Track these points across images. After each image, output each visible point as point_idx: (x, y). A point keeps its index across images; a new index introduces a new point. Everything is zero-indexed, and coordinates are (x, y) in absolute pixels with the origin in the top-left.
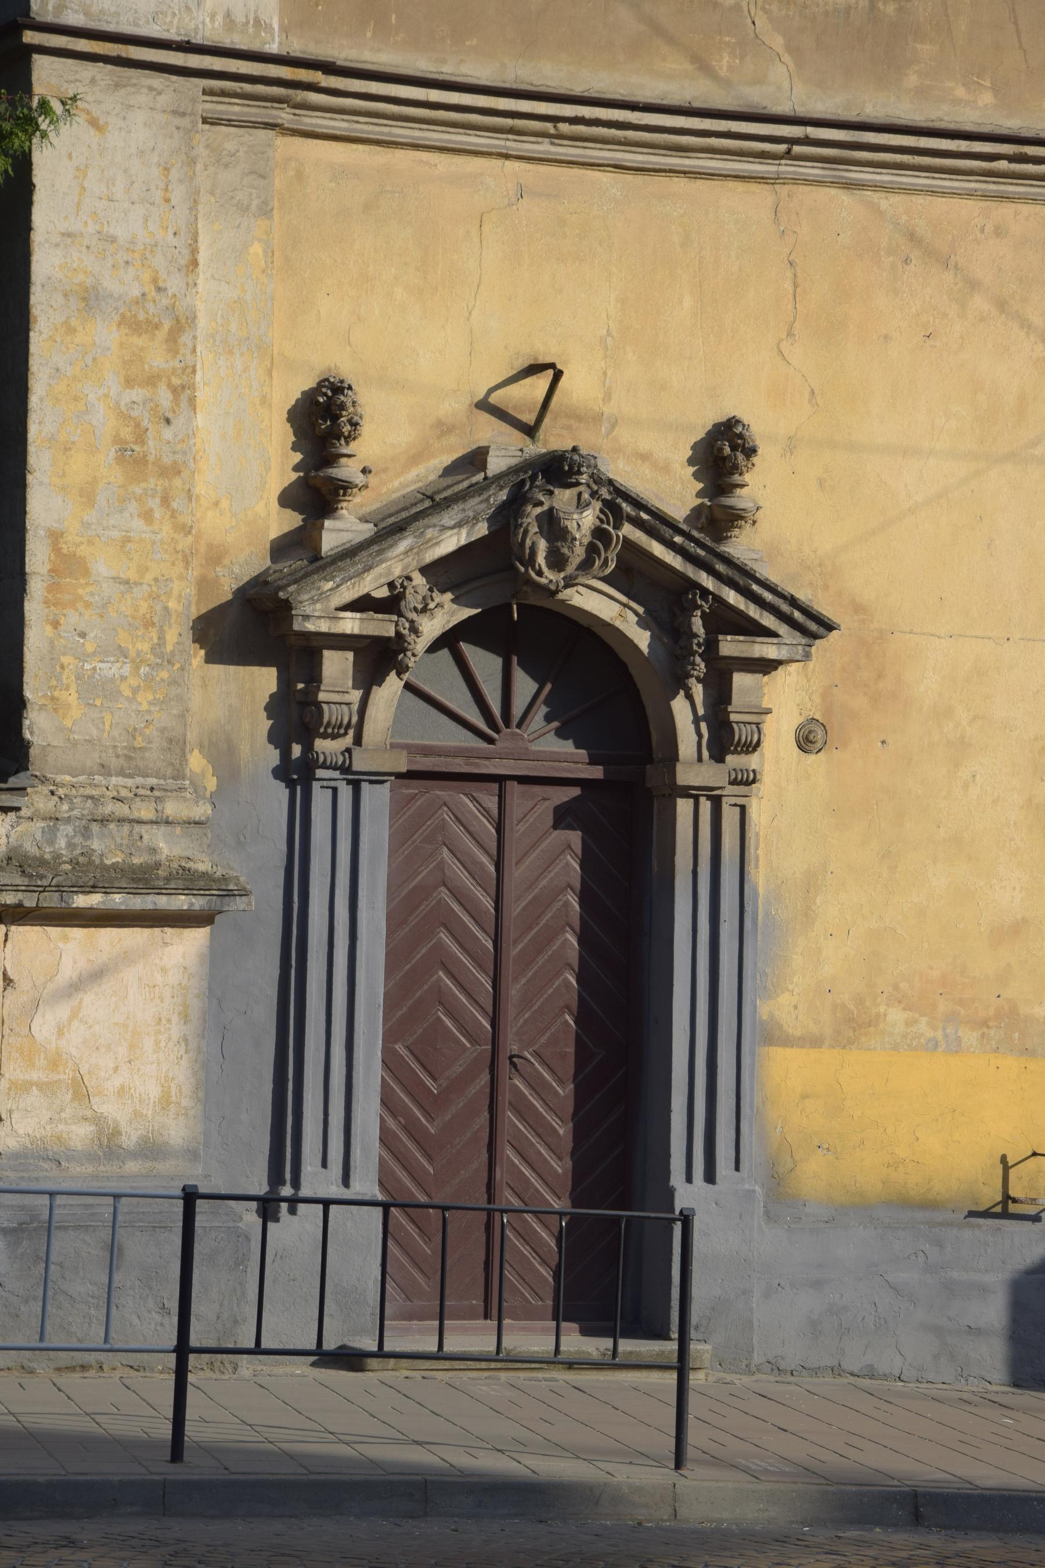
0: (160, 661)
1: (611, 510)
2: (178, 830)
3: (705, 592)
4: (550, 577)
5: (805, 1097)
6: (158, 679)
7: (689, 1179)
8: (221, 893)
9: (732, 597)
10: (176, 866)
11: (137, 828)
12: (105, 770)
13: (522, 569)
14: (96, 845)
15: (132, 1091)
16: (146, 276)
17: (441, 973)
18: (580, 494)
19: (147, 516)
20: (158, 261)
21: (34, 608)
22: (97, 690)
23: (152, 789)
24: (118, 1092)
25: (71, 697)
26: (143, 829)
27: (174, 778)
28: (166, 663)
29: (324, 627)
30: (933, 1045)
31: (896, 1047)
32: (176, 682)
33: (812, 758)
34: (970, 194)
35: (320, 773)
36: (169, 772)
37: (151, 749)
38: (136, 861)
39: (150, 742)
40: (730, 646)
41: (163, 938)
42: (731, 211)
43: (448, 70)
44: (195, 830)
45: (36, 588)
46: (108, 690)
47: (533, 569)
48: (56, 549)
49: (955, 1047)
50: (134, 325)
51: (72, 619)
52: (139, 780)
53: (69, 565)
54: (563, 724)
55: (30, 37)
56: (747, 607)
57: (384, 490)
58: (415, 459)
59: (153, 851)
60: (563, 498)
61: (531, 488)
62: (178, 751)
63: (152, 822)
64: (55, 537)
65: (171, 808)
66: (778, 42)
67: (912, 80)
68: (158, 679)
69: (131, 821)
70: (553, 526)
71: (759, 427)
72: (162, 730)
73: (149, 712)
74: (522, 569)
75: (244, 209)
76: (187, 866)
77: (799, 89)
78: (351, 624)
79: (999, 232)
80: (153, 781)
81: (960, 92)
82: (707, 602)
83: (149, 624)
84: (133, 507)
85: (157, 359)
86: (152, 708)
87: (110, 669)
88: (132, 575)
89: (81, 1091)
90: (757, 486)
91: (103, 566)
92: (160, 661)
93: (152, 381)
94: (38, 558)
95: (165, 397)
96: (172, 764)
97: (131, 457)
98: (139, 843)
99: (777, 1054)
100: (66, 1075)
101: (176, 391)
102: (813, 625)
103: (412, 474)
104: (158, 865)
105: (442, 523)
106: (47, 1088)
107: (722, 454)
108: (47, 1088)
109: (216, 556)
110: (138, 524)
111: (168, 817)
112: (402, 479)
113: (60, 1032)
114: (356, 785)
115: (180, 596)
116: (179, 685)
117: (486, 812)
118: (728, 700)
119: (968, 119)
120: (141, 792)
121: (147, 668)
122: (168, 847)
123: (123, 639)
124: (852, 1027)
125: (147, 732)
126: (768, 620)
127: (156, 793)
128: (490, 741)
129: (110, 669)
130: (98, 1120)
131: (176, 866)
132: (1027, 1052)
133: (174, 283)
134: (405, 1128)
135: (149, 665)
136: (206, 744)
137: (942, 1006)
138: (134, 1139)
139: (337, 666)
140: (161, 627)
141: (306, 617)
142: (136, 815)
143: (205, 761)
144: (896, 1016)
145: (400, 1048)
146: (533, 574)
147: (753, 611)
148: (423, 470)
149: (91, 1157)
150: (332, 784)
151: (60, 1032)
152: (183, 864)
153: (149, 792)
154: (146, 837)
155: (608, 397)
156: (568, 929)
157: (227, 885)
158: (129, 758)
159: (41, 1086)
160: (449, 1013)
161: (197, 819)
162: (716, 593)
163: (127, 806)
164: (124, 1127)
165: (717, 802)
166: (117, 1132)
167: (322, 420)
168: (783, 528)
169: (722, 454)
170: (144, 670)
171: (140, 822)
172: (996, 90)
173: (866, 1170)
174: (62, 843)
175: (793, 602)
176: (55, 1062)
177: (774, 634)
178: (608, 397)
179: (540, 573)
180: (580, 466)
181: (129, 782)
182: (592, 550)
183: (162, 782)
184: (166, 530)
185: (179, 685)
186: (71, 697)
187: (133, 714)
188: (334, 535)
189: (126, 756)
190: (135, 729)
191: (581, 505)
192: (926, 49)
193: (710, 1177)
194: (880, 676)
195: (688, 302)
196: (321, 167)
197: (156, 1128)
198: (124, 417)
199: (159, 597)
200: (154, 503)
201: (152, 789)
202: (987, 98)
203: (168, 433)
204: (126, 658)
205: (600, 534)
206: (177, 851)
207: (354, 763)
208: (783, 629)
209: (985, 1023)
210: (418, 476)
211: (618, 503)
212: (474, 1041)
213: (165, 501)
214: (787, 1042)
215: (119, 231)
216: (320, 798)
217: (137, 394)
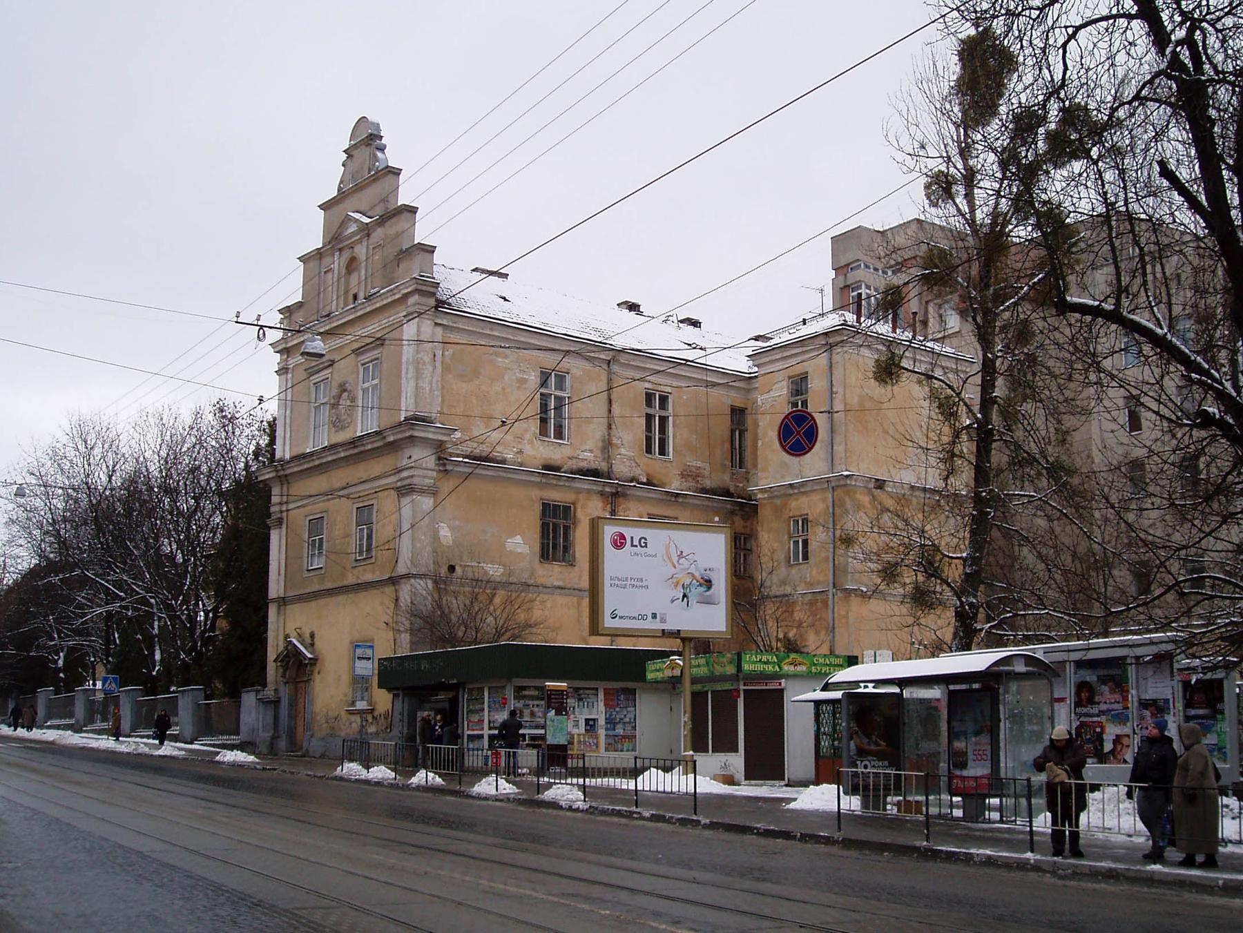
169: (312, 636)
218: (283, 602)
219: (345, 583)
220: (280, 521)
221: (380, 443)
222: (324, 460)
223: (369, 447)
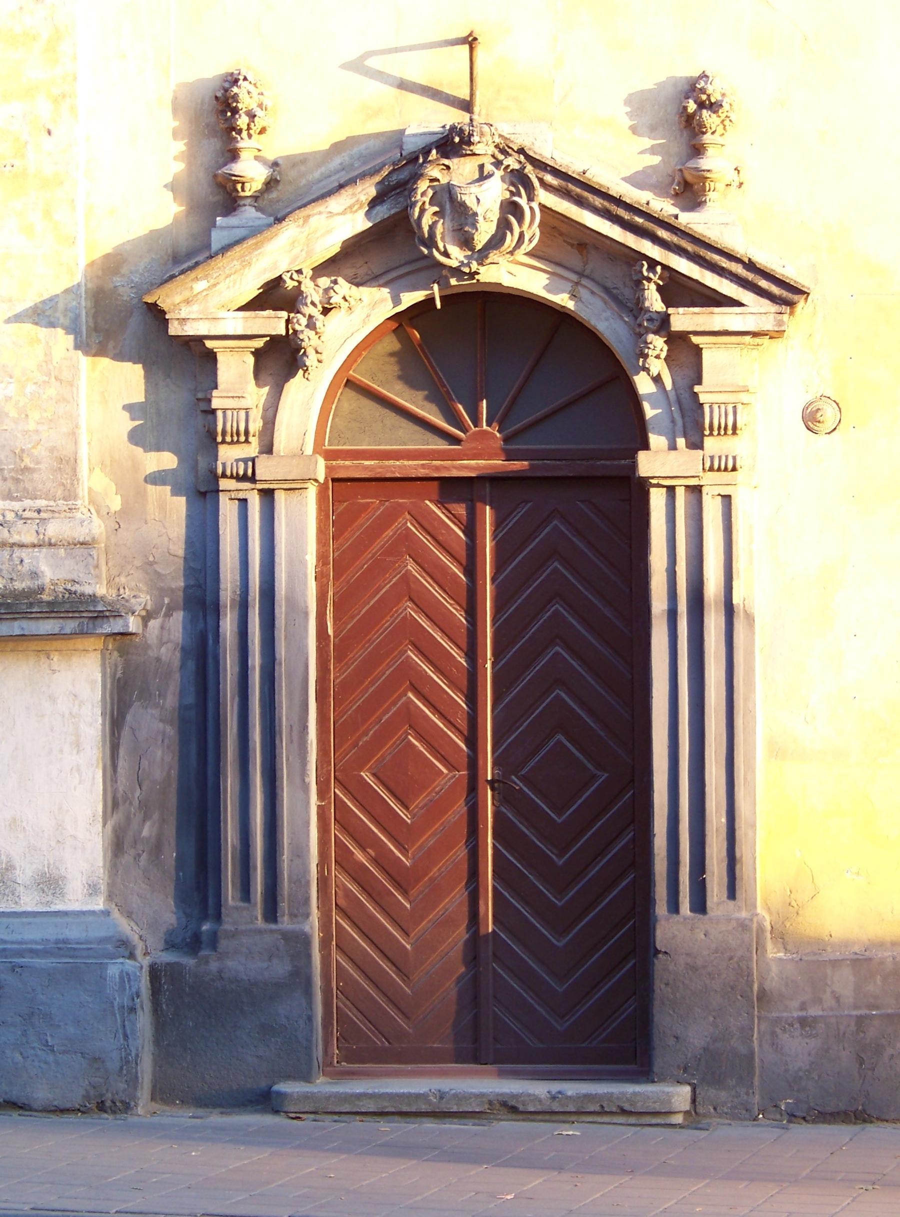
0: (47, 379)
1: (519, 179)
2: (62, 551)
3: (653, 264)
4: (457, 256)
6: (45, 397)
7: (674, 907)
8: (90, 615)
10: (61, 589)
11: (18, 553)
13: (426, 251)
15: (24, 824)
17: (410, 695)
18: (481, 167)
23: (39, 511)
24: (10, 825)
26: (24, 553)
27: (65, 499)
28: (53, 380)
32: (64, 399)
33: (822, 439)
35: (224, 484)
36: (59, 493)
37: (40, 469)
38: (19, 585)
39: (38, 463)
40: (683, 319)
41: (50, 665)
44: (79, 551)
47: (438, 249)
52: (28, 503)
54: (685, 436)
56: (703, 276)
57: (304, 182)
59: (34, 575)
60: (461, 171)
61: (424, 162)
62: (69, 470)
63: (34, 546)
65: (53, 530)
68: (45, 397)
69: (13, 545)
70: (449, 201)
72: (52, 450)
73: (37, 431)
74: (426, 251)
76: (73, 589)
78: (238, 323)
80: (41, 503)
82: (655, 273)
86: (40, 428)
92: (47, 379)
96: (63, 484)
98: (19, 567)
102: (786, 294)
104: (41, 589)
105: (328, 210)
111: (50, 539)
112: (323, 169)
114: (268, 495)
115: (66, 310)
116: (68, 402)
117: (455, 518)
118: (699, 382)
120: (27, 514)
121: (34, 387)
125: (35, 452)
127: (43, 515)
128: (456, 440)
131: (61, 589)
134: (375, 861)
135: (35, 383)
136: (108, 462)
138: (29, 873)
139: (235, 371)
140: (47, 343)
141: (183, 321)
142: (16, 538)
143: (107, 480)
146: (436, 254)
148: (347, 158)
150: (241, 495)
152: (69, 587)
153: (35, 515)
154: (26, 561)
156: (558, 641)
157: (95, 606)
158: (17, 481)
160: (421, 737)
161: (81, 540)
162: (664, 262)
163: (6, 530)
164: (17, 861)
165: (696, 491)
169: (688, 115)
170: (30, 388)
171: (22, 546)
175: (751, 266)
177: (739, 304)
179: (446, 254)
180: (470, 135)
181: (17, 506)
182: (504, 226)
183: (52, 503)
185: (68, 402)
187: (19, 435)
188: (225, 233)
189: (13, 478)
190: (23, 451)
191: (483, 176)
193: (700, 905)
197: (52, 862)
199: (44, 312)
201: (39, 511)
204: (11, 377)
205: (511, 209)
206: (62, 574)
207: (257, 472)
210: (341, 164)
211: (525, 170)
212: (451, 767)
216: (228, 510)
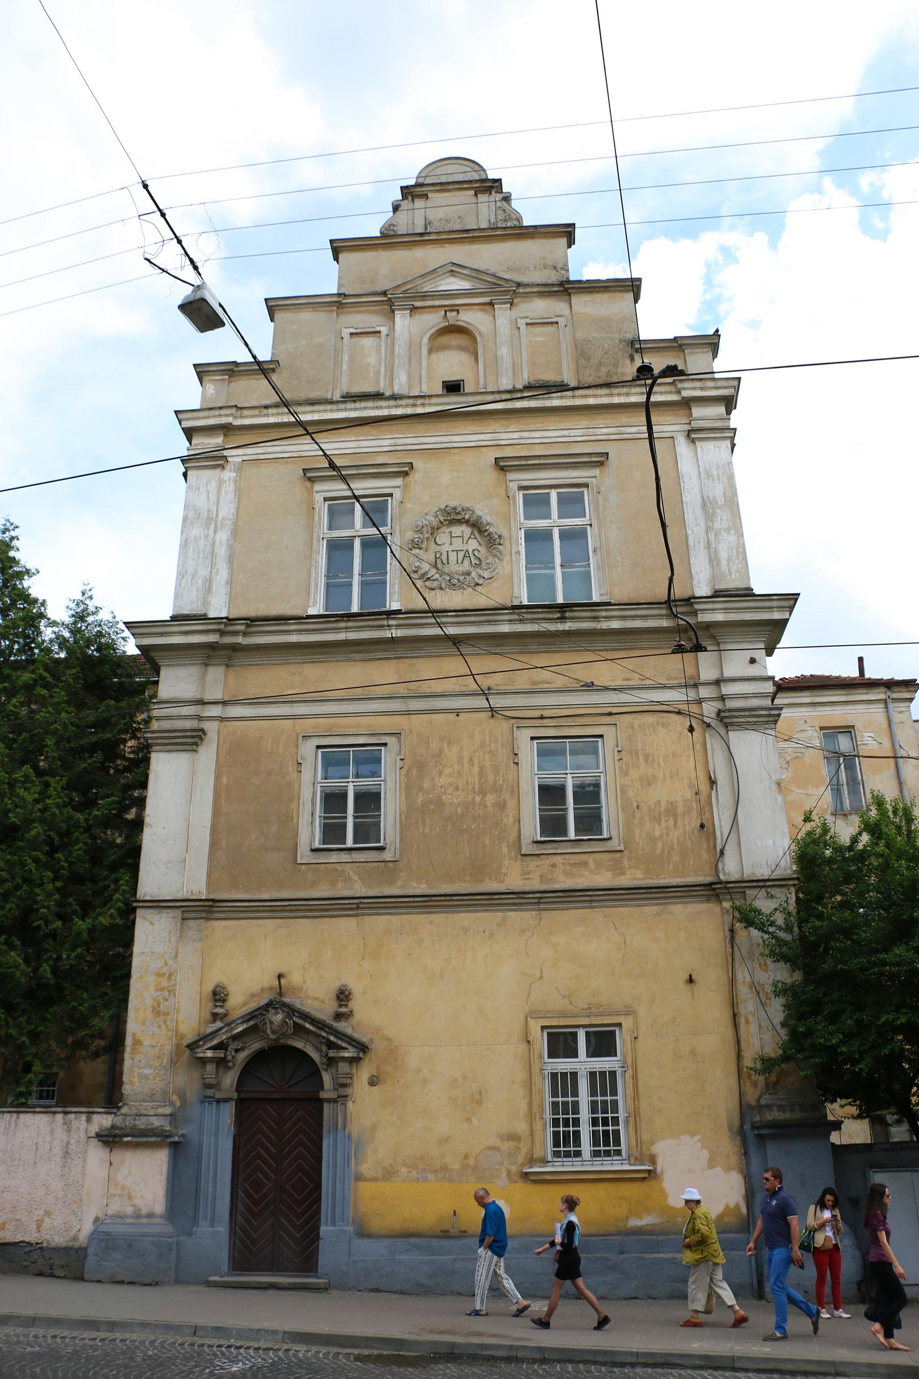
5: (372, 1198)
9: (332, 1038)
12: (144, 1101)
14: (137, 1123)
16: (163, 961)
19: (160, 1027)
20: (167, 957)
21: (127, 1056)
22: (143, 1077)
25: (136, 1080)
29: (201, 1055)
30: (418, 1180)
31: (404, 1181)
34: (421, 913)
42: (345, 927)
43: (256, 897)
45: (128, 1049)
46: (146, 1077)
48: (134, 1038)
49: (425, 1180)
50: (159, 975)
51: (137, 1057)
53: (137, 1043)
55: (135, 904)
58: (244, 1004)
64: (134, 1035)
66: (356, 878)
67: (399, 883)
71: (356, 987)
75: (194, 941)
77: (363, 889)
78: (209, 1054)
79: (431, 922)
81: (415, 885)
83: (159, 1058)
84: (156, 1025)
85: (165, 983)
87: (147, 1071)
88: (154, 1044)
89: (130, 1197)
90: (356, 1004)
91: (146, 1042)
93: (163, 989)
94: (129, 1041)
95: (166, 994)
97: (156, 1011)
99: (362, 1185)
100: (126, 1192)
101: (169, 992)
103: (243, 1009)
106: (120, 1196)
107: (343, 996)
108: (120, 1196)
109: (182, 1037)
110: (157, 1029)
113: (125, 1178)
119: (418, 892)
122: (157, 1122)
123: (152, 1062)
124: (389, 1174)
126: (344, 1045)
129: (147, 1071)
130: (134, 1206)
132: (451, 1181)
133: (171, 962)
137: (421, 1166)
144: (404, 1170)
145: (246, 1185)
147: (339, 1042)
149: (132, 1217)
151: (125, 1178)
155: (304, 982)
159: (119, 1195)
166: (140, 1210)
167: (219, 996)
168: (366, 1017)
169: (343, 996)
172: (427, 883)
173: (392, 1222)
174: (127, 1123)
176: (123, 1188)
178: (304, 982)
184: (164, 1031)
186: (136, 1080)
192: (403, 874)
194: (396, 1060)
195: (330, 952)
196: (219, 928)
198: (155, 1000)
200: (161, 1023)
202: (424, 885)
203: (167, 1003)
208: (349, 1047)
209: (436, 1171)
213: (165, 1023)
214: (366, 1180)
215: (156, 950)
217: (158, 993)
218: (197, 910)
219: (494, 887)
220: (191, 740)
221: (665, 623)
222: (604, 625)
223: (615, 625)
